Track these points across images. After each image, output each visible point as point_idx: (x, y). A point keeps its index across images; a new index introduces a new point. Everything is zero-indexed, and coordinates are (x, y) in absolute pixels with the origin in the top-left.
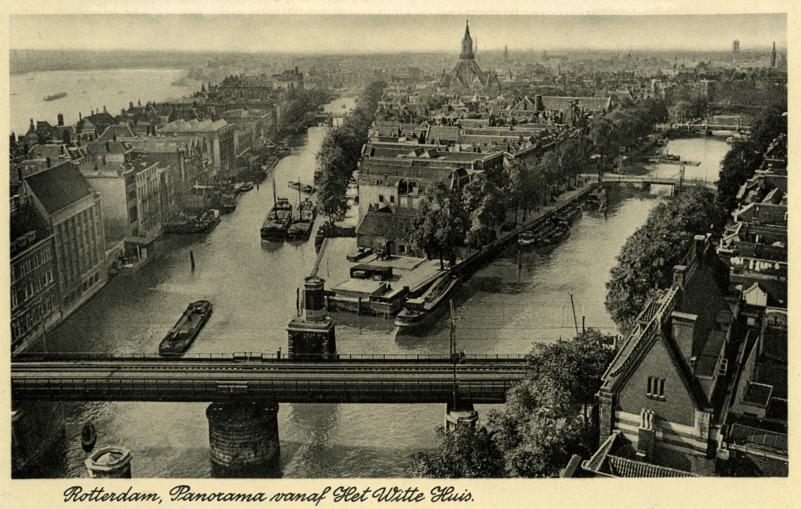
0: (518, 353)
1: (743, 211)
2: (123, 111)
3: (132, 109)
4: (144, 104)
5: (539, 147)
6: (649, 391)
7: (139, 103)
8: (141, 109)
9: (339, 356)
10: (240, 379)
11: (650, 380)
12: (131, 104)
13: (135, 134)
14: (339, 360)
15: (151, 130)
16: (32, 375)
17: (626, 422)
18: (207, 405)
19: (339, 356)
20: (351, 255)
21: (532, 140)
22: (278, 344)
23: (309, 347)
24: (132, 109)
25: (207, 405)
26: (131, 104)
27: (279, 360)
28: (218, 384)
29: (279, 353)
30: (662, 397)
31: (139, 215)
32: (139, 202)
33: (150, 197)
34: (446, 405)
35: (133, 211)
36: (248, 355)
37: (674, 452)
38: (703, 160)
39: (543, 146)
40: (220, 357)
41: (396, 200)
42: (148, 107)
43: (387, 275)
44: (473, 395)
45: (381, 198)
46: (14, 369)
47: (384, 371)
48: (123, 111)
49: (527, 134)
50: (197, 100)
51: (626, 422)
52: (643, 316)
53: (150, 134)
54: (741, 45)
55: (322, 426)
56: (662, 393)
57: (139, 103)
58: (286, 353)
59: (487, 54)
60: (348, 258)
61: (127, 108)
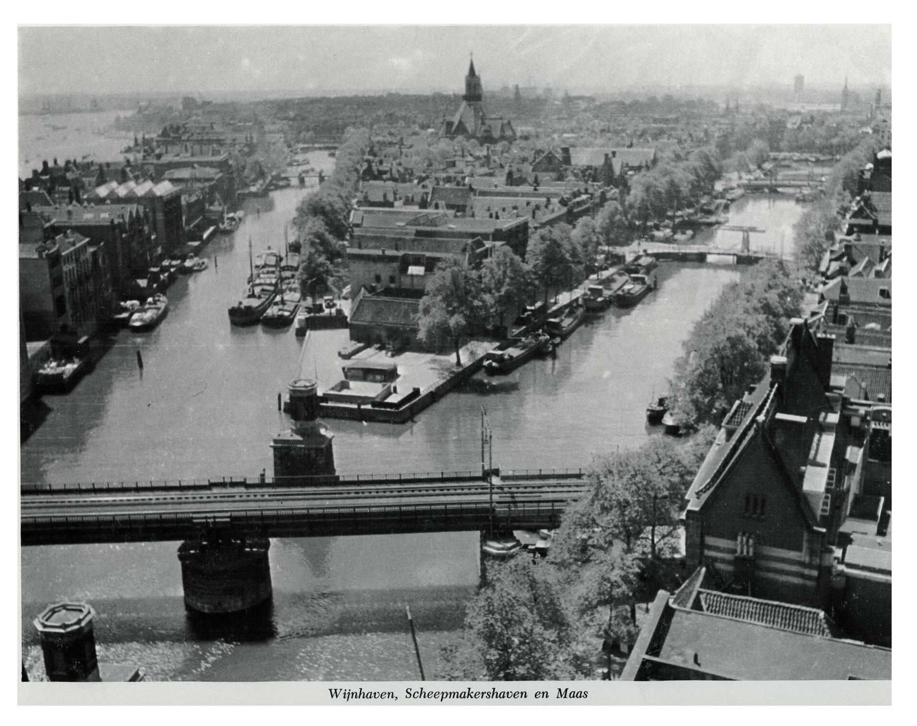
0: (222, 475)
1: (827, 287)
2: (35, 172)
3: (46, 169)
4: (61, 163)
5: (570, 212)
6: (747, 510)
7: (55, 161)
8: (60, 169)
9: (338, 477)
10: (220, 508)
11: (748, 498)
12: (45, 163)
13: (55, 202)
14: (336, 482)
15: (74, 196)
16: (287, 504)
17: (717, 549)
18: (179, 543)
19: (338, 477)
20: (343, 353)
21: (563, 202)
22: (263, 464)
23: (302, 463)
24: (46, 169)
25: (179, 543)
26: (45, 163)
27: (262, 484)
28: (192, 518)
29: (263, 476)
30: (763, 517)
31: (68, 306)
32: (67, 289)
33: (80, 282)
34: (478, 533)
35: (60, 302)
36: (228, 480)
37: (777, 581)
38: (773, 227)
39: (575, 210)
40: (370, 479)
41: (397, 280)
42: (67, 168)
43: (390, 375)
44: (514, 520)
45: (378, 278)
46: (24, 507)
47: (444, 492)
48: (35, 172)
49: (556, 195)
50: (131, 157)
51: (717, 549)
52: (732, 418)
53: (74, 202)
54: (806, 81)
55: (317, 563)
56: (763, 514)
57: (55, 161)
58: (270, 477)
59: (493, 95)
60: (340, 354)
61: (40, 168)
